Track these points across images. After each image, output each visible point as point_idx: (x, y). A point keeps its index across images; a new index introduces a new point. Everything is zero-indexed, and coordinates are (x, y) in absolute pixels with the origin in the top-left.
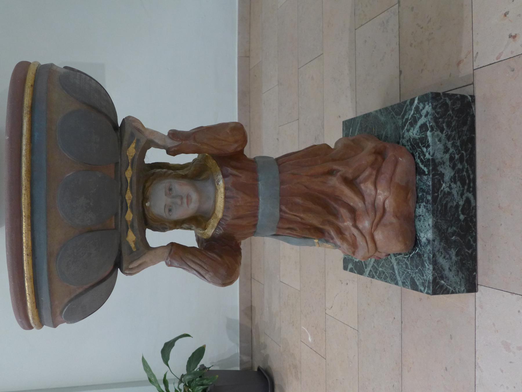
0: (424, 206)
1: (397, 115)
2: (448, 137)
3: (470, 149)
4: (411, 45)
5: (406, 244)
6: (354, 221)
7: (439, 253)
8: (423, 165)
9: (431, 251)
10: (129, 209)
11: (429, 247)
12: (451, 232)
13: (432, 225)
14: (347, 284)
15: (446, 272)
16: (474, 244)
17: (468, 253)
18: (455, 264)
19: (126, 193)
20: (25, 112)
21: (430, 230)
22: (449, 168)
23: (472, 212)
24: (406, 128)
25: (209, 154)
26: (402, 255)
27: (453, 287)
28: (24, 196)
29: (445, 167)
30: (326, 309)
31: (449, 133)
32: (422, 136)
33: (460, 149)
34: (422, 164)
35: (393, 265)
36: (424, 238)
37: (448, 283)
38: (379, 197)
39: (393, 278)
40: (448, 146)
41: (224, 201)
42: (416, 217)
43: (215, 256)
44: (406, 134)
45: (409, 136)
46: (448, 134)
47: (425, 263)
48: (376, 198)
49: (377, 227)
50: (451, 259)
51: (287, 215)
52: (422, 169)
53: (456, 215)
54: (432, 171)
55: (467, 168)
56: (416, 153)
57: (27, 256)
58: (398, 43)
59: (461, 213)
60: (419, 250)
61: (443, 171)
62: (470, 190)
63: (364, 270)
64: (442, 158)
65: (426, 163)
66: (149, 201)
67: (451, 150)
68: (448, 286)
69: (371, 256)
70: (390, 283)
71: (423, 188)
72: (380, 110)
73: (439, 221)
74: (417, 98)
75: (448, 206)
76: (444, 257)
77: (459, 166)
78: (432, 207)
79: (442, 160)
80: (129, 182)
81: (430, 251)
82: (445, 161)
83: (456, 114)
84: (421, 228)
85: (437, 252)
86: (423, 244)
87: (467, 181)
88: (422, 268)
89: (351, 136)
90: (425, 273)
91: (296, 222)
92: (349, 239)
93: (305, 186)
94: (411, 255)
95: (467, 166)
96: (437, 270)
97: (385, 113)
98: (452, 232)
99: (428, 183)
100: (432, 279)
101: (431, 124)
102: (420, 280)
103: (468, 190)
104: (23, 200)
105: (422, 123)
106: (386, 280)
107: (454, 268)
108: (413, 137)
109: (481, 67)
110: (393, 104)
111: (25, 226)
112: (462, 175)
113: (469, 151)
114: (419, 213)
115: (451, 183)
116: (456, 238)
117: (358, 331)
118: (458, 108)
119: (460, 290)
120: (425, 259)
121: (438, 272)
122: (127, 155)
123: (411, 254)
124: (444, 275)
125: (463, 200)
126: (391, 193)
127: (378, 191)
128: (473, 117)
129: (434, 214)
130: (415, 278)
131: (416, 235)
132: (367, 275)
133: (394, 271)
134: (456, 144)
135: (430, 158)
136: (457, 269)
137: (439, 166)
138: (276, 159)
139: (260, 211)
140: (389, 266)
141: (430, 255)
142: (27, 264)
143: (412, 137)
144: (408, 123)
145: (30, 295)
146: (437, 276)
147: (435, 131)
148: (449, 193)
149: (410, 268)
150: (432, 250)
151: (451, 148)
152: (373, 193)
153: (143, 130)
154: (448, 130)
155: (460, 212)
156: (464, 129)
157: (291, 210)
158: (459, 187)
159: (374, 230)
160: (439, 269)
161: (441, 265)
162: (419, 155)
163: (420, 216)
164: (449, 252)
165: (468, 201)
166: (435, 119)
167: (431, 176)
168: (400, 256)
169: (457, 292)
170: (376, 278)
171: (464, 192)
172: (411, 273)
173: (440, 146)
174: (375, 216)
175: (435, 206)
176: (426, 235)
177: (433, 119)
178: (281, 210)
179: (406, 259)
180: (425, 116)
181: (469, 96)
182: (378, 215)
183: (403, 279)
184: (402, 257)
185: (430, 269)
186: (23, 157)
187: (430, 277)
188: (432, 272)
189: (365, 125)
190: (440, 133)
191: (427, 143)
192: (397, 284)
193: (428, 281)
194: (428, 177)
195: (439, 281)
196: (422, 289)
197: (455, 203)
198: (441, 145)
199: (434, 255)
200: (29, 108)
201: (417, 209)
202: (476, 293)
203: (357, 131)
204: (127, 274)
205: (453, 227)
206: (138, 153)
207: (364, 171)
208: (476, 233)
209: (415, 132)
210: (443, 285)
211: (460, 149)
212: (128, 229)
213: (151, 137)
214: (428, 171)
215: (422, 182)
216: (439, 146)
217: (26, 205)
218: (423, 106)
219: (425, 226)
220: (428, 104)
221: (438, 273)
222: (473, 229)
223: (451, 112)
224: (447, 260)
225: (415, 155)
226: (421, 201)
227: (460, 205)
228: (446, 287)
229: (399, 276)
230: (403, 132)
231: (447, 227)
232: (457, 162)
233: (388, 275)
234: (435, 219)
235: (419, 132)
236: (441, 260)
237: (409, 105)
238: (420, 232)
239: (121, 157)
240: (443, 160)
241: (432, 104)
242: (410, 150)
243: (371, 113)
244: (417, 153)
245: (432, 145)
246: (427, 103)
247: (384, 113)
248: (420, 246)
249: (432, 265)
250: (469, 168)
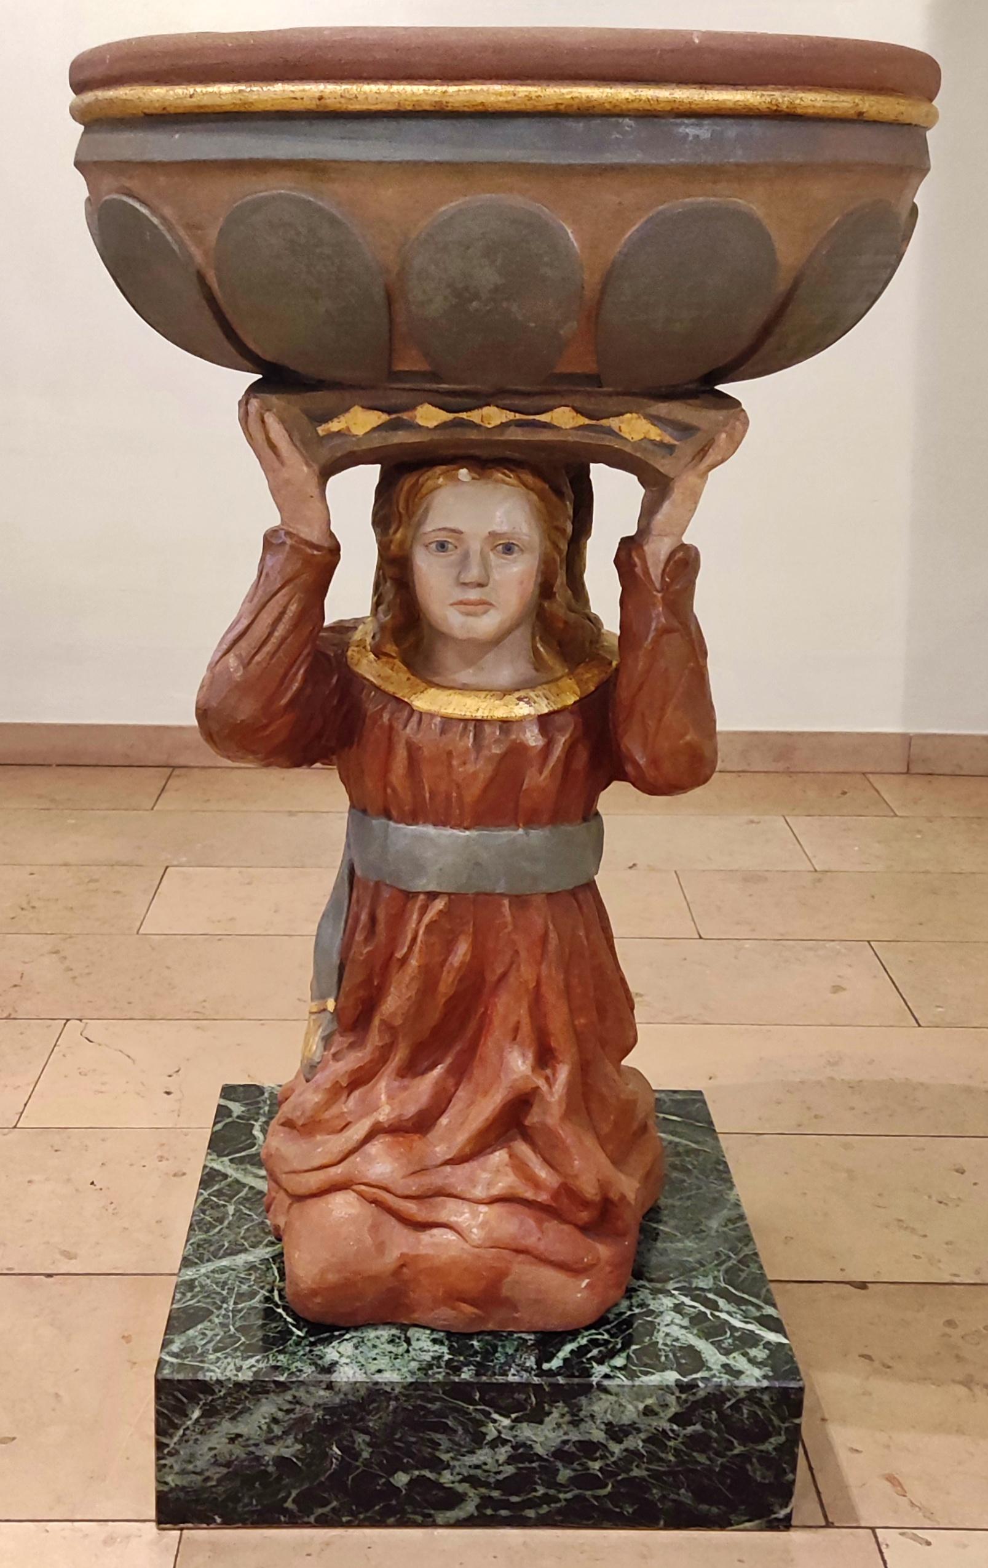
0: (440, 1357)
1: (726, 1272)
2: (657, 1439)
3: (618, 1510)
4: (950, 1323)
5: (314, 1293)
6: (396, 1129)
7: (290, 1402)
8: (569, 1356)
9: (298, 1377)
10: (451, 416)
11: (309, 1371)
12: (354, 1442)
13: (380, 1380)
14: (168, 1093)
15: (227, 1427)
16: (312, 1519)
17: (285, 1499)
18: (252, 1456)
19: (503, 408)
20: (777, 94)
21: (365, 1373)
22: (559, 1440)
23: (414, 1513)
24: (687, 1301)
25: (617, 670)
26: (280, 1281)
27: (177, 1447)
28: (508, 92)
29: (564, 1426)
30: (80, 1020)
31: (671, 1443)
32: (663, 1353)
33: (620, 1478)
34: (572, 1352)
35: (245, 1250)
36: (338, 1355)
37: (194, 1431)
38: (466, 1210)
39: (204, 1249)
40: (630, 1438)
41: (466, 717)
42: (404, 1328)
43: (295, 686)
44: (668, 1302)
45: (662, 1310)
46: (670, 1440)
47: (258, 1357)
48: (463, 1199)
49: (371, 1202)
50: (269, 1442)
51: (415, 916)
52: (559, 1350)
53: (410, 1460)
54: (550, 1385)
55: (559, 1500)
56: (607, 1331)
57: (317, 95)
58: (957, 1280)
59: (414, 1477)
60: (298, 1336)
61: (550, 1421)
62: (486, 1508)
63: (227, 1155)
64: (592, 1416)
65: (577, 1365)
66: (473, 478)
67: (616, 1448)
68: (181, 1432)
69: (276, 1182)
70: (187, 1241)
71: (497, 1355)
72: (742, 1217)
73: (393, 1403)
74: (785, 1341)
75: (439, 1436)
76: (275, 1420)
77: (564, 1474)
78: (438, 1383)
79: (586, 1419)
80: (537, 417)
81: (298, 1373)
82: (582, 1426)
83: (734, 1467)
84: (370, 1344)
85: (295, 1397)
86: (318, 1349)
87: (514, 1499)
88: (242, 1348)
89: (657, 1117)
90: (226, 1358)
91: (393, 942)
92: (334, 1110)
93: (504, 975)
94: (280, 1310)
95: (566, 1500)
96: (235, 1396)
97: (733, 1233)
98: (356, 1446)
99: (513, 1371)
100: (207, 1379)
101: (701, 1384)
102: (202, 1339)
103: (486, 1501)
104: (497, 88)
105: (703, 1356)
106: (196, 1228)
107: (238, 1451)
108: (659, 1324)
109: (881, 1552)
110: (763, 1258)
111: (413, 94)
112: (536, 1483)
113: (611, 1506)
114: (418, 1340)
115: (512, 1447)
116: (334, 1460)
117: (15, 1127)
118: (751, 1473)
119: (167, 1470)
120: (271, 1356)
121: (229, 1399)
122: (622, 414)
123: (284, 1310)
124: (218, 1420)
125: (456, 1484)
126: (477, 1250)
127: (483, 1209)
128: (722, 1523)
129: (416, 1390)
130: (209, 1324)
131: (348, 1330)
132: (210, 1165)
133: (227, 1254)
134: (635, 1464)
135: (594, 1380)
136: (236, 1462)
137: (566, 1409)
138: (594, 881)
139: (430, 830)
140: (242, 1238)
141: (286, 1375)
142: (292, 95)
143: (657, 1320)
144: (703, 1309)
145: (193, 99)
146: (215, 1397)
147: (678, 1398)
148: (478, 1440)
149: (240, 1306)
150: (300, 1379)
151: (623, 1446)
152: (479, 1192)
153: (703, 466)
154: (680, 1440)
155: (417, 1473)
156: (683, 1491)
157: (428, 927)
158: (499, 1473)
159: (361, 1194)
160: (238, 1404)
161: (249, 1409)
162: (602, 1342)
163: (408, 1341)
164: (292, 1436)
165: (453, 1499)
166: (717, 1398)
167: (536, 1380)
168: (276, 1274)
169: (163, 1462)
170: (202, 1194)
171: (482, 1486)
172: (223, 1312)
173: (631, 1412)
174: (407, 1197)
175: (441, 1392)
176: (348, 1361)
177: (717, 1393)
178: (432, 896)
179: (267, 1294)
180: (728, 1365)
181: (788, 1510)
182: (411, 1208)
183: (204, 1283)
184: (274, 1282)
185: (240, 1374)
186: (632, 91)
187: (213, 1374)
188: (229, 1379)
189: (692, 1164)
190: (673, 1409)
191: (641, 1372)
192: (186, 1262)
193: (201, 1365)
194: (533, 1373)
195: (201, 1403)
196: (175, 1348)
197: (445, 1457)
198: (635, 1415)
199: (283, 1387)
200: (787, 107)
201: (428, 1332)
202: (154, 1524)
203: (670, 1138)
204: (244, 403)
205: (370, 1450)
206: (628, 449)
207: (548, 1162)
208: (348, 1525)
209: (676, 1331)
210: (186, 1416)
211: (620, 1478)
212: (389, 413)
213: (677, 494)
214: (550, 1370)
215: (516, 1350)
216: (630, 1407)
217: (480, 99)
218: (759, 1360)
219: (375, 1359)
220: (765, 1377)
221: (224, 1397)
222: (362, 1516)
223: (738, 1449)
224: (265, 1427)
225: (601, 1331)
226: (455, 1344)
227: (440, 1474)
228: (181, 1425)
229: (213, 1272)
230: (673, 1292)
231: (372, 1431)
232: (579, 1468)
233: (214, 1235)
234: (400, 1393)
235: (674, 1343)
236: (267, 1408)
237: (762, 1315)
238: (355, 1341)
239: (618, 394)
240: (586, 1422)
241: (767, 1388)
242: (617, 1312)
243: (732, 1186)
244: (606, 1336)
245: (634, 1386)
246: (771, 1374)
247: (734, 1230)
248: (310, 1342)
249: (251, 1379)
250: (558, 1505)
